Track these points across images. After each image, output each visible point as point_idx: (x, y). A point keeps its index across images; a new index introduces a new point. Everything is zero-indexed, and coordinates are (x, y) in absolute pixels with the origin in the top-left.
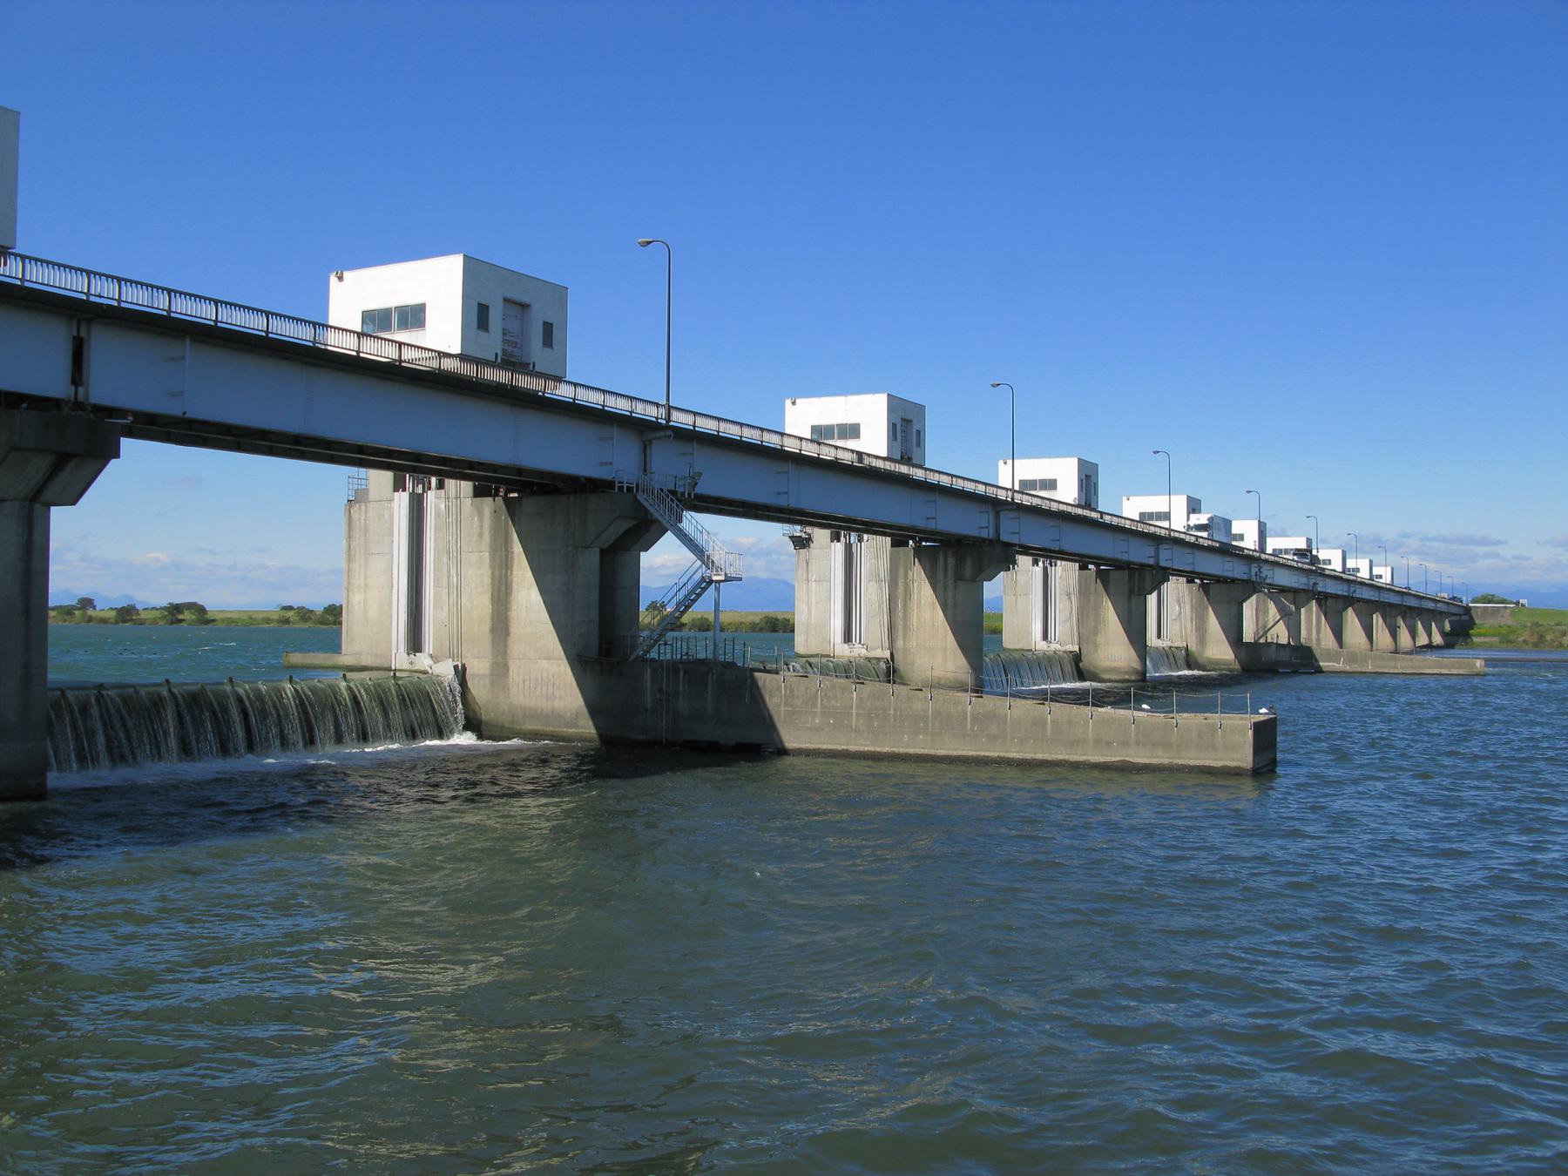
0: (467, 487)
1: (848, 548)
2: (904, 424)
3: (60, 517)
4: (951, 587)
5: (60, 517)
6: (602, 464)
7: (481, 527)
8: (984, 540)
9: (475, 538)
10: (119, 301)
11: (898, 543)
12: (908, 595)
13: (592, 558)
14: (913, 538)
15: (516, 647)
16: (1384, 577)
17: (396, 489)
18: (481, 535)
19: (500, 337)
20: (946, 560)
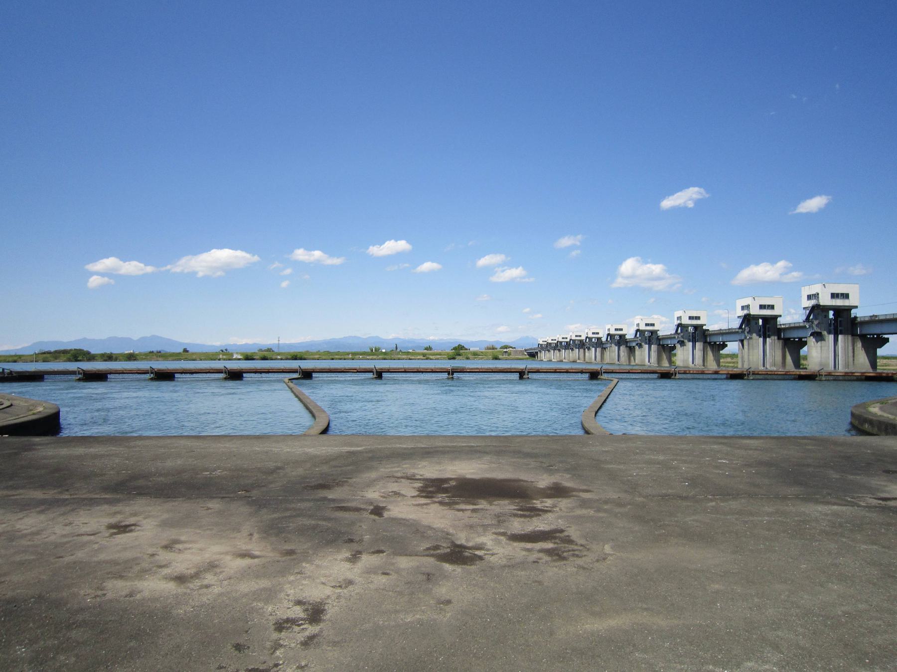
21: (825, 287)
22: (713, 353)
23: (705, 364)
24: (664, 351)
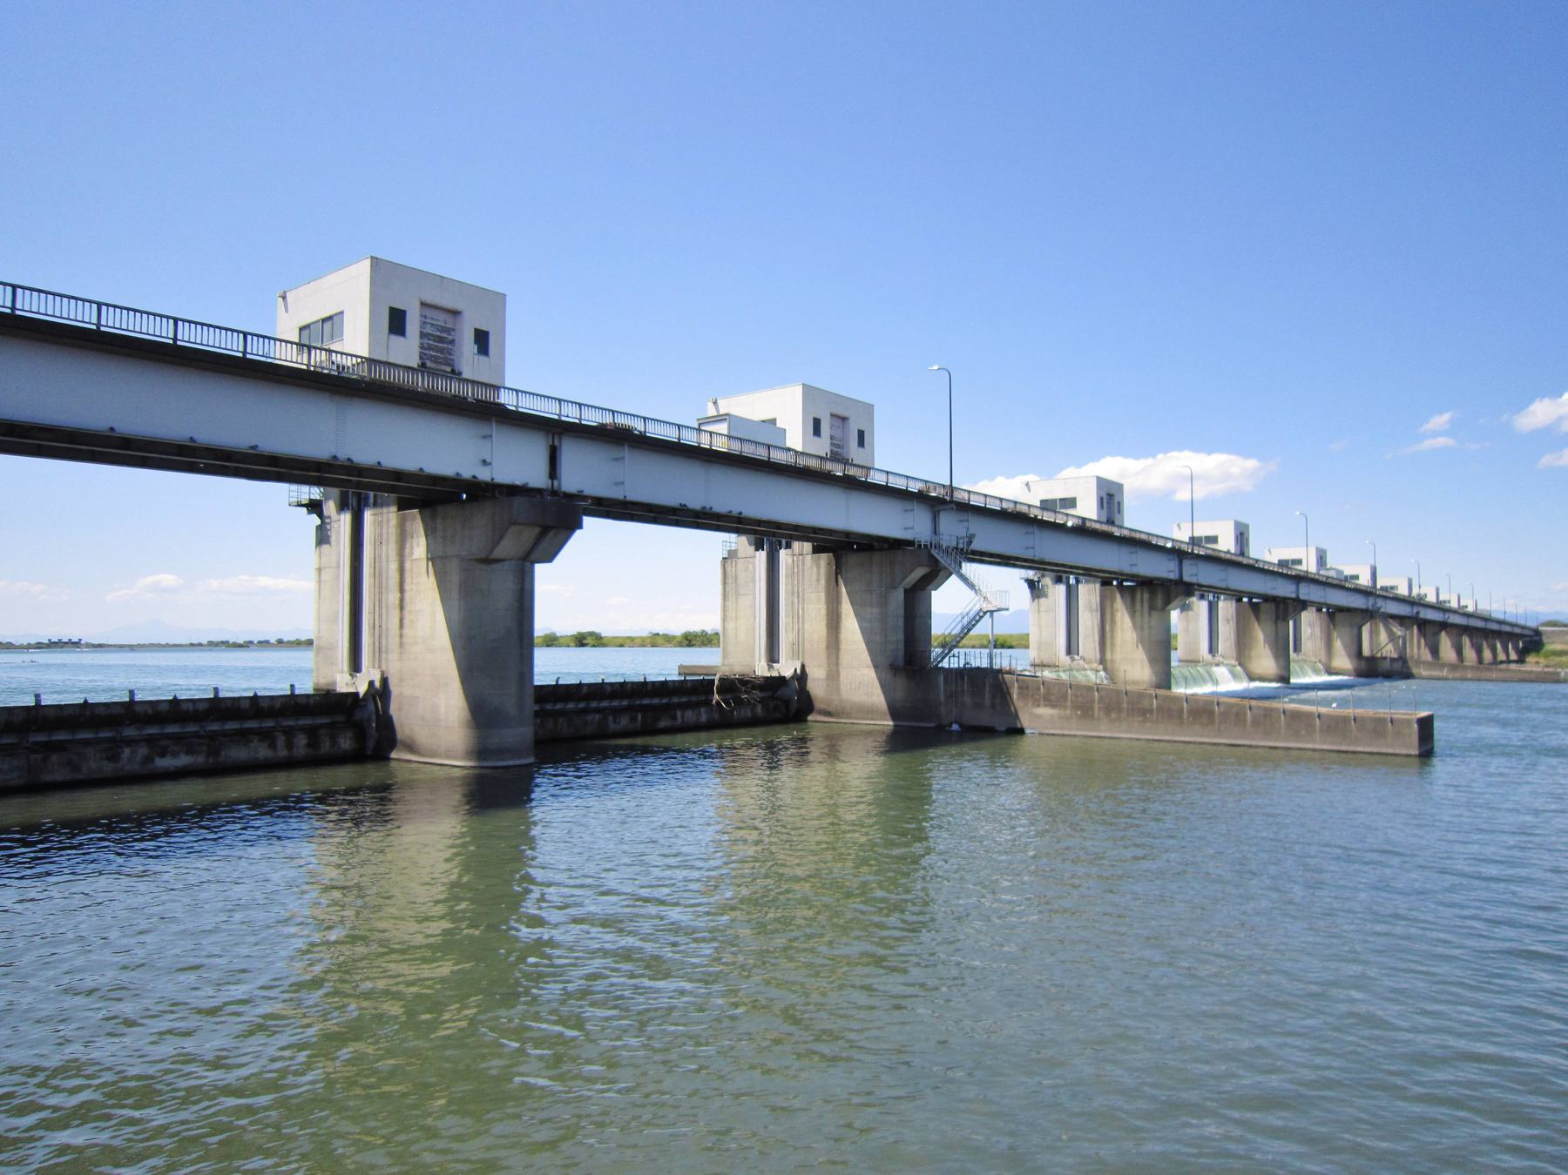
0: (808, 546)
1: (1210, 604)
2: (838, 423)
3: (539, 569)
4: (1146, 615)
5: (539, 569)
6: (906, 529)
7: (818, 574)
8: (1171, 581)
9: (814, 583)
10: (580, 419)
11: (1106, 583)
12: (1113, 622)
13: (899, 596)
14: (1117, 579)
15: (845, 658)
16: (1304, 562)
17: (757, 550)
18: (818, 580)
19: (829, 441)
20: (1142, 595)
21: (1029, 490)
22: (1132, 615)
23: (1108, 656)
24: (1258, 619)
